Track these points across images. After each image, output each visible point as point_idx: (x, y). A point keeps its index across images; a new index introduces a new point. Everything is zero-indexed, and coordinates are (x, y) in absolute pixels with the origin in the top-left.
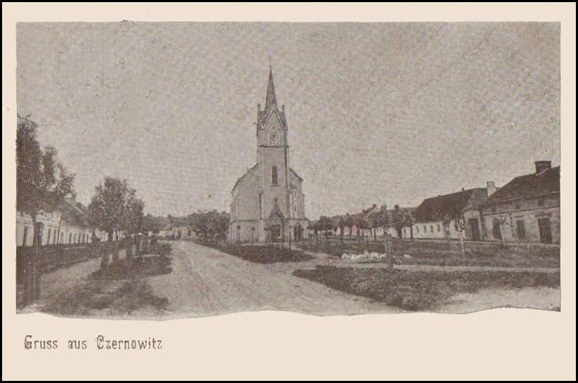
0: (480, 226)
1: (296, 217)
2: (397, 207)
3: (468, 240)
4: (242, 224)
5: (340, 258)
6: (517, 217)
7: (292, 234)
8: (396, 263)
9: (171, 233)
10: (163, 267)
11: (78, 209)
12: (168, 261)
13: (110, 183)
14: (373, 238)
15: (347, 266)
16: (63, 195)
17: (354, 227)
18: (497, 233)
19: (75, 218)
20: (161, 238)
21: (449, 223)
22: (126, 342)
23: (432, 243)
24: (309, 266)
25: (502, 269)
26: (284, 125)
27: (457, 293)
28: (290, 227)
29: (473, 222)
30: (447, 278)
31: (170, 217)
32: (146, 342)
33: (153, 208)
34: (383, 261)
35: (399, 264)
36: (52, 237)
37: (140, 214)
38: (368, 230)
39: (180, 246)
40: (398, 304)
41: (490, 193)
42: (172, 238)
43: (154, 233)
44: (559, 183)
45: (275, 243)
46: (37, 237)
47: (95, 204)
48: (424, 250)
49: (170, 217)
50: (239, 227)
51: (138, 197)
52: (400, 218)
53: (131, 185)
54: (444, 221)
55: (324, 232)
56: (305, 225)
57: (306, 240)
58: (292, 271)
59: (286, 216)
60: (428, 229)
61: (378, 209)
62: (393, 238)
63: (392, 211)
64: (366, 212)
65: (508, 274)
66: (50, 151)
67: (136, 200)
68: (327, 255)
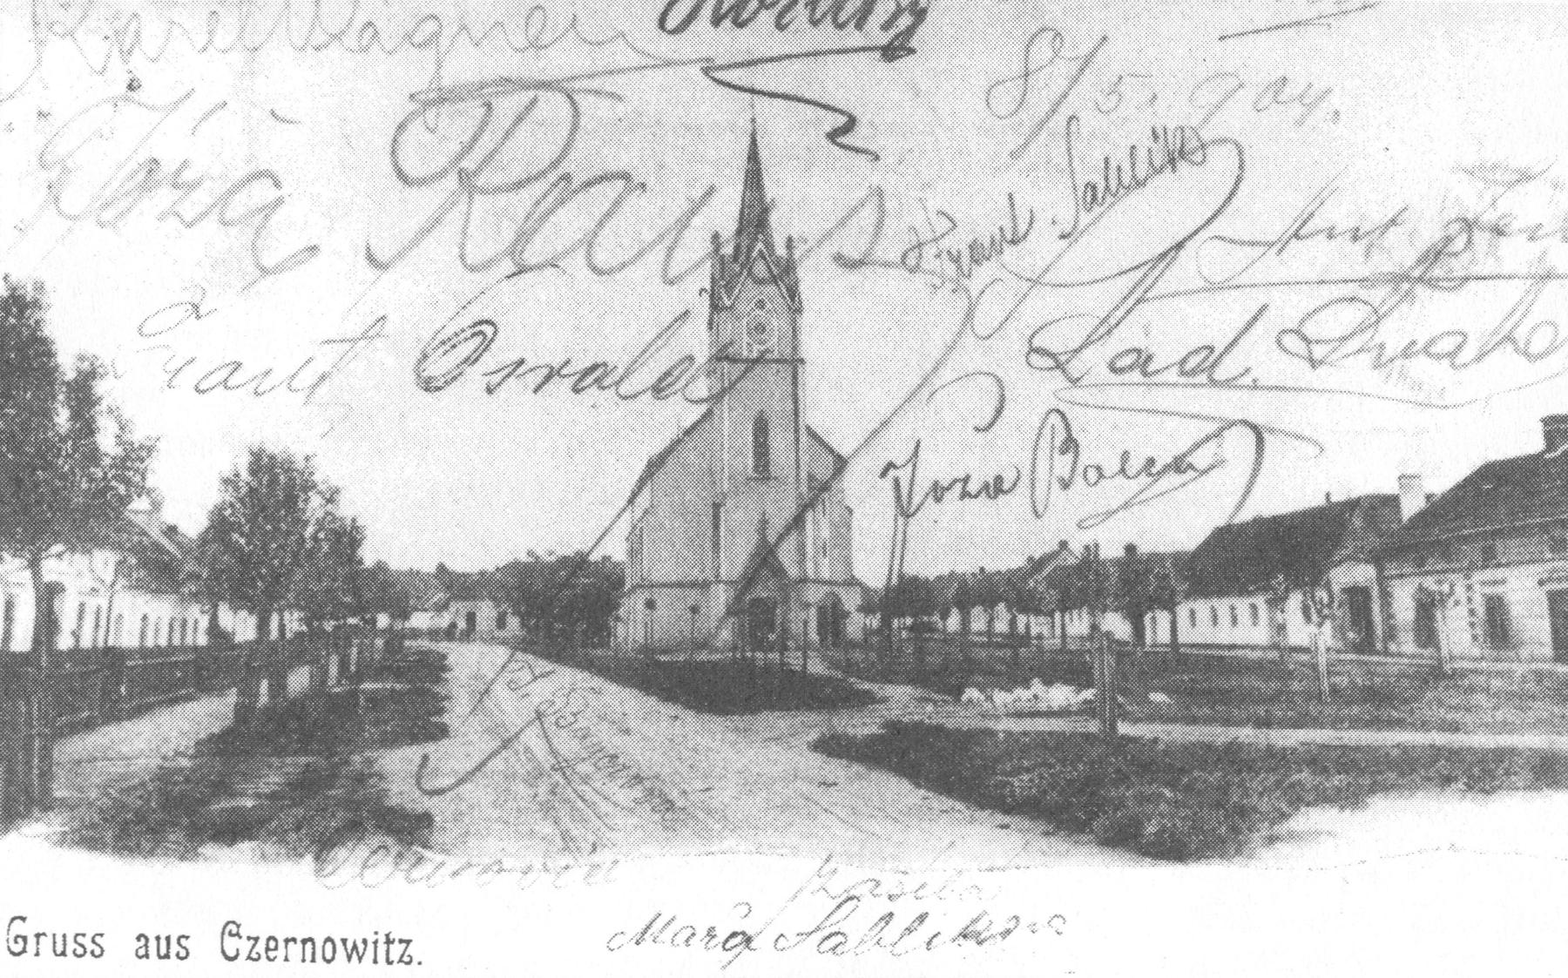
0: (1376, 607)
1: (826, 575)
2: (1130, 549)
3: (1338, 652)
4: (662, 598)
5: (958, 700)
6: (1483, 583)
7: (813, 625)
8: (1125, 716)
9: (444, 621)
10: (422, 721)
11: (164, 541)
12: (437, 705)
13: (262, 464)
14: (1058, 641)
15: (977, 723)
16: (124, 501)
17: (1001, 607)
18: (1426, 630)
19: (158, 568)
20: (415, 634)
21: (1284, 599)
22: (304, 942)
23: (1222, 658)
24: (862, 725)
25: (1439, 738)
26: (792, 298)
27: (1303, 809)
28: (807, 606)
29: (1357, 598)
30: (1279, 759)
31: (442, 568)
32: (365, 942)
33: (396, 543)
34: (1088, 710)
35: (1136, 721)
36: (102, 632)
37: (352, 559)
38: (1042, 619)
39: (469, 662)
40: (1126, 838)
41: (1411, 506)
42: (449, 633)
43: (393, 617)
44: (1293, 516)
45: (759, 655)
46: (47, 623)
47: (220, 526)
48: (1208, 679)
49: (442, 568)
50: (650, 605)
51: (346, 509)
52: (1142, 582)
53: (326, 472)
54: (1270, 595)
55: (909, 621)
56: (851, 600)
57: (853, 645)
58: (814, 735)
59: (793, 572)
60: (1224, 617)
61: (1071, 553)
62: (1118, 642)
63: (1117, 562)
64: (1037, 565)
65: (1454, 754)
66: (86, 366)
67: (342, 519)
68: (919, 692)
